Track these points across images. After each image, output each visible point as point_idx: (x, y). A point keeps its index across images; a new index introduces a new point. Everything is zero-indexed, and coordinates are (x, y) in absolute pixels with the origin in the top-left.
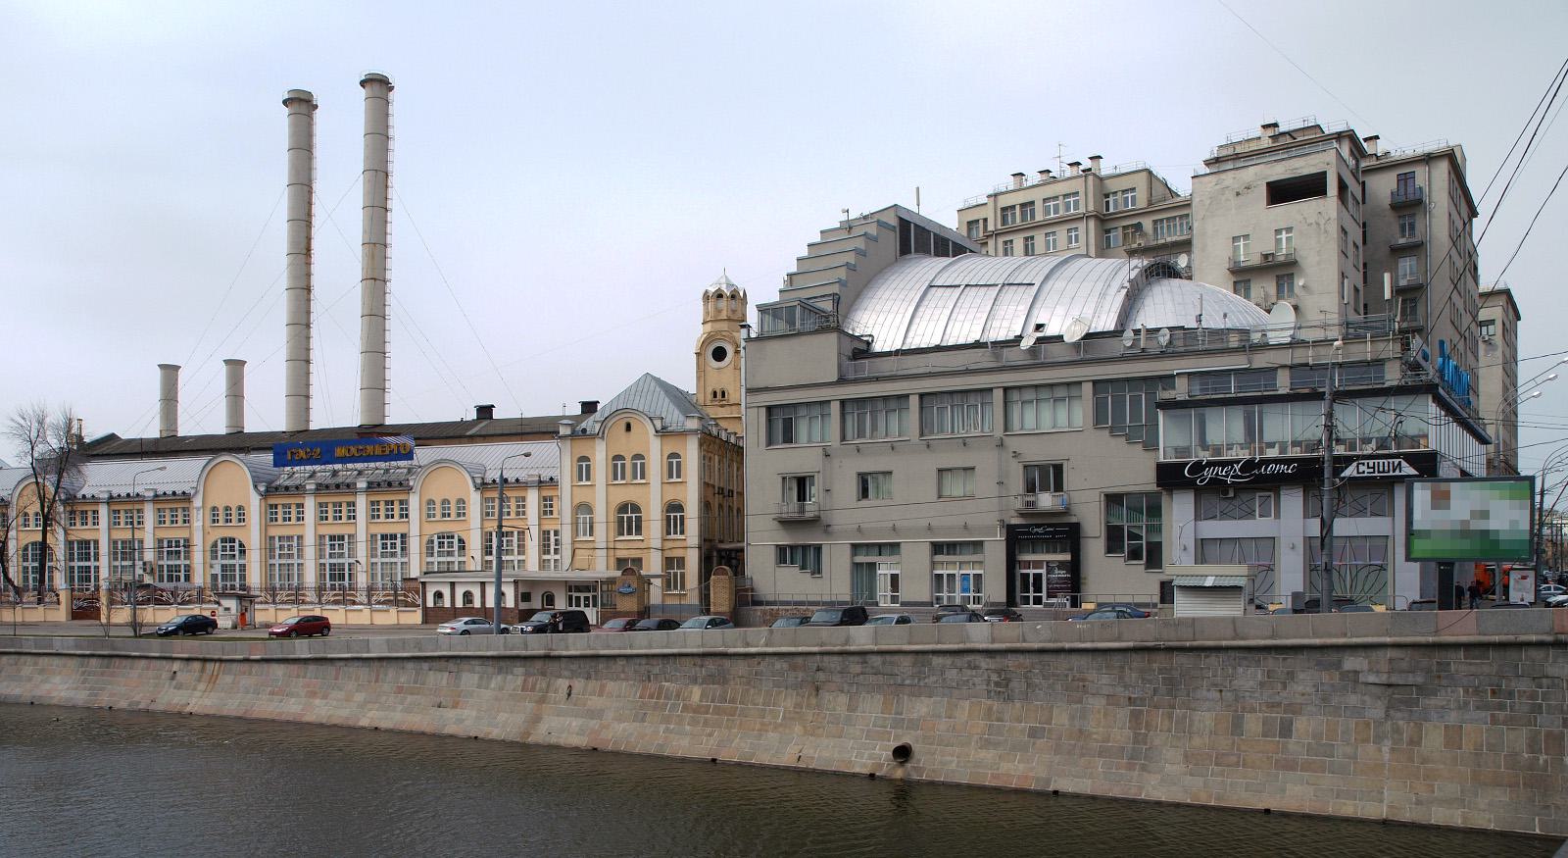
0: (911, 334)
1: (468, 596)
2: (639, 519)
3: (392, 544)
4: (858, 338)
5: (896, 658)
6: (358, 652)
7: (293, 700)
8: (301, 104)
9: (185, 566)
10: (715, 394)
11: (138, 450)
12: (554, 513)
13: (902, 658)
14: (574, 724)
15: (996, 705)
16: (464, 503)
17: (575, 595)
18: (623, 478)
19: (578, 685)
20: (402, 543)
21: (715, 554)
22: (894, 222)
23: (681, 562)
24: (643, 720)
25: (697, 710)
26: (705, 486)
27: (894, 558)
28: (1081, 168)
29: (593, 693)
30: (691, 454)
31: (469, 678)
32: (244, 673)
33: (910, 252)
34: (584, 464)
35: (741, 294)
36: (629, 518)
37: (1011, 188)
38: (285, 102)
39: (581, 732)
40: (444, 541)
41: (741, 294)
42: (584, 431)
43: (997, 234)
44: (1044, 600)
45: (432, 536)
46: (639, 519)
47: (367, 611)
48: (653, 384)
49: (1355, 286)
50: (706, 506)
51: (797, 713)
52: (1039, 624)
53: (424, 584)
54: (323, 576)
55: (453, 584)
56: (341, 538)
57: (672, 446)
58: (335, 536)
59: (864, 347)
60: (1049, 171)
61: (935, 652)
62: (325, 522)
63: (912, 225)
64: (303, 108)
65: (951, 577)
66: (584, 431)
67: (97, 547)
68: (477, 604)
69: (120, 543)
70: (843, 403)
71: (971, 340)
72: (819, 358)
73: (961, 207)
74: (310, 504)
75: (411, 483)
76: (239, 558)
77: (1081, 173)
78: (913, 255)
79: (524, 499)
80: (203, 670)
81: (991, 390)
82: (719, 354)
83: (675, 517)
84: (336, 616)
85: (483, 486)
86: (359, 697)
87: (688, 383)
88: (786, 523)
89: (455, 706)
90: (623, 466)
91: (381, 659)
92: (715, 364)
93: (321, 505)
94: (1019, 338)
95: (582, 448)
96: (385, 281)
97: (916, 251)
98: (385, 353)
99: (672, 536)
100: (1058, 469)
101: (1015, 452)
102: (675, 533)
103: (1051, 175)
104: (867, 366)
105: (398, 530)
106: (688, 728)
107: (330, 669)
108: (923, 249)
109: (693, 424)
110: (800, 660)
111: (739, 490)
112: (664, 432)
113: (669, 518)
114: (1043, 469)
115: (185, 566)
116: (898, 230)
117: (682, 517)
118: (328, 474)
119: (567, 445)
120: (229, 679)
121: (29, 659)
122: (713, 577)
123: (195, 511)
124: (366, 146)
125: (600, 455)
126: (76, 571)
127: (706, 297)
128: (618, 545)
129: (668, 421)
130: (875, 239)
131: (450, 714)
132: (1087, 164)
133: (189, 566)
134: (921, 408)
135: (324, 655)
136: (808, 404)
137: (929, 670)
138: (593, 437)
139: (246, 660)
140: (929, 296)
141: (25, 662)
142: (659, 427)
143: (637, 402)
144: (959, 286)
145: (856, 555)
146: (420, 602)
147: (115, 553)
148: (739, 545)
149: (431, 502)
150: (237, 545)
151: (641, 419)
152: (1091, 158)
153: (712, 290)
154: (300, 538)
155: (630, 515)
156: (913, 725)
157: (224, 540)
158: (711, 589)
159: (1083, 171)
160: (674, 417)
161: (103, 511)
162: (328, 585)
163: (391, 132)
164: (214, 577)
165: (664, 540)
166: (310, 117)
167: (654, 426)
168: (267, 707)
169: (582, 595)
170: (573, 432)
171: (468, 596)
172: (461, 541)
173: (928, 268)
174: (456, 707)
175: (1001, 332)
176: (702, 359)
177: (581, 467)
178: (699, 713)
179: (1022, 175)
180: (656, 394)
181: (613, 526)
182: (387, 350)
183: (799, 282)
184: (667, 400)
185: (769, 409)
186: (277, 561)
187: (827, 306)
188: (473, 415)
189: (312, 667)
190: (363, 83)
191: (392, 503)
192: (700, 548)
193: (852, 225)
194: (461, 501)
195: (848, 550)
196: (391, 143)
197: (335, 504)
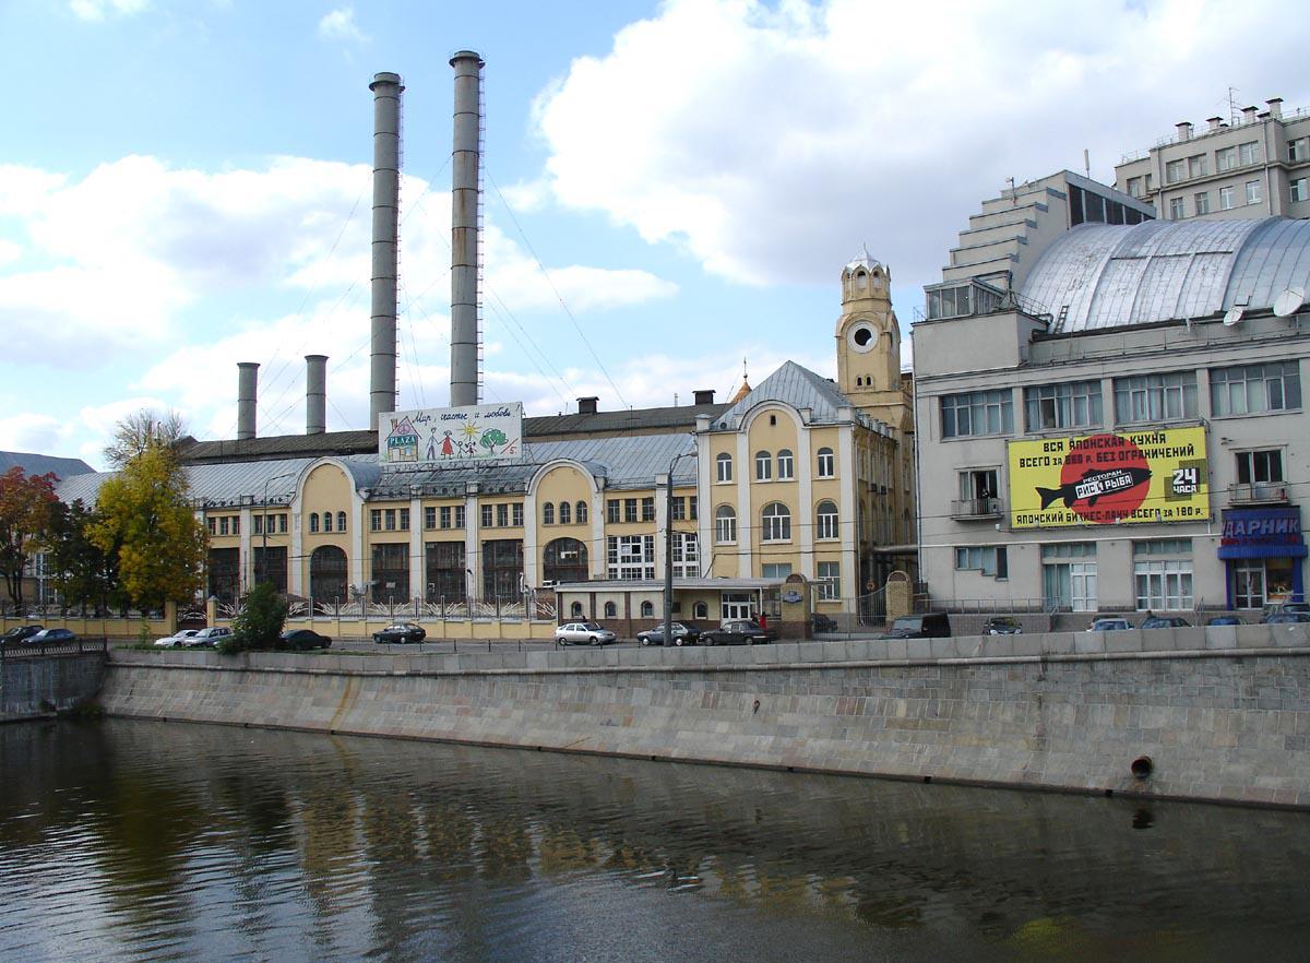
0: (1095, 312)
1: (610, 607)
2: (786, 521)
4: (1036, 318)
5: (1129, 665)
6: (514, 667)
7: (444, 717)
8: (388, 87)
9: (647, 569)
11: (216, 453)
13: (1135, 665)
14: (764, 743)
15: (1245, 715)
16: (586, 506)
17: (730, 604)
18: (768, 476)
19: (766, 701)
21: (871, 558)
22: (1065, 189)
23: (835, 566)
24: (843, 737)
25: (903, 725)
26: (861, 483)
27: (1089, 560)
28: (1258, 113)
29: (784, 709)
30: (844, 446)
31: (641, 696)
32: (387, 690)
34: (724, 462)
36: (776, 520)
37: (1176, 140)
38: (372, 87)
39: (773, 749)
42: (724, 425)
43: (1162, 192)
44: (1265, 602)
46: (787, 522)
47: (495, 623)
48: (797, 373)
49: (1037, 489)
50: (861, 505)
51: (1018, 726)
52: (1290, 626)
53: (560, 594)
55: (593, 595)
57: (823, 439)
59: (1042, 327)
60: (1219, 119)
61: (1171, 658)
63: (1083, 192)
64: (391, 91)
65: (1155, 578)
66: (724, 425)
68: (621, 615)
70: (1026, 390)
71: (1164, 318)
72: (995, 342)
73: (1119, 163)
77: (1258, 119)
78: (1085, 224)
80: (242, 678)
81: (1194, 371)
82: (862, 337)
83: (828, 518)
84: (433, 630)
86: (518, 714)
87: (829, 369)
89: (627, 723)
90: (768, 463)
91: (539, 674)
94: (1221, 314)
95: (722, 444)
96: (476, 267)
97: (1088, 220)
99: (825, 539)
100: (1276, 455)
101: (1224, 439)
102: (828, 535)
103: (1222, 122)
104: (1049, 349)
106: (895, 744)
107: (483, 687)
108: (1095, 216)
109: (846, 415)
110: (1020, 669)
111: (891, 486)
112: (813, 425)
113: (820, 519)
114: (1260, 457)
116: (1068, 197)
117: (733, 522)
120: (371, 695)
121: (158, 672)
122: (889, 583)
124: (457, 126)
125: (742, 452)
127: (846, 276)
128: (818, 548)
129: (816, 412)
130: (1045, 209)
131: (622, 732)
132: (1264, 108)
134: (1116, 394)
136: (1075, 384)
137: (1167, 677)
138: (736, 431)
139: (390, 675)
140: (1111, 271)
141: (155, 677)
142: (807, 421)
143: (779, 392)
144: (1145, 257)
145: (1045, 556)
146: (555, 613)
148: (912, 547)
149: (549, 506)
151: (783, 409)
152: (1269, 102)
153: (853, 266)
155: (776, 516)
156: (1152, 735)
158: (887, 596)
159: (1260, 116)
160: (823, 407)
163: (482, 110)
165: (815, 544)
166: (396, 99)
168: (412, 725)
169: (739, 605)
171: (610, 607)
173: (1112, 237)
174: (629, 726)
175: (1194, 308)
177: (721, 465)
178: (906, 728)
179: (1189, 124)
180: (801, 384)
181: (758, 533)
182: (479, 340)
183: (964, 258)
184: (813, 390)
185: (943, 399)
187: (1000, 284)
189: (462, 682)
190: (453, 62)
191: (433, 509)
192: (856, 551)
193: (1018, 193)
194: (581, 505)
195: (1036, 552)
196: (482, 121)
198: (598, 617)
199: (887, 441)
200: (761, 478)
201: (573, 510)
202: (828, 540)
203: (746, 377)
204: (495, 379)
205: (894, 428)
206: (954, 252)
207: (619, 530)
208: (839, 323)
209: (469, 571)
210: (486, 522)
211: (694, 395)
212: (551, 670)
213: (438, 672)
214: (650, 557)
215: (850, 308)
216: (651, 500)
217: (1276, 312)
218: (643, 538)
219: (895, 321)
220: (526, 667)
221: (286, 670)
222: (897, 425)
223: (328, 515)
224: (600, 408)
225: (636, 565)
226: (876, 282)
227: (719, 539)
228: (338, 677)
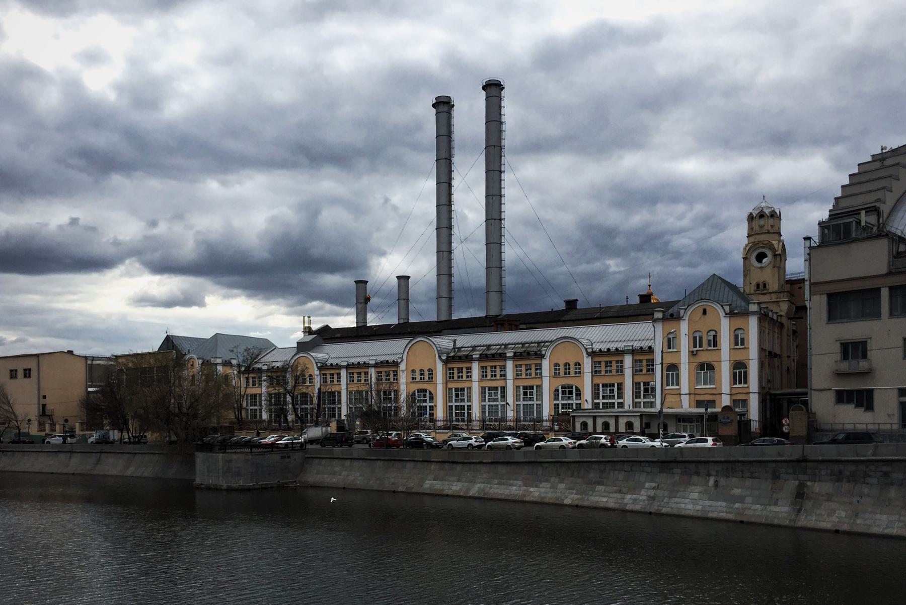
3: (530, 392)
9: (468, 406)
10: (758, 286)
12: (464, 377)
16: (580, 365)
18: (701, 346)
19: (722, 481)
20: (618, 389)
26: (761, 350)
33: (433, 413)
35: (778, 214)
40: (568, 391)
41: (778, 214)
45: (558, 387)
53: (574, 417)
54: (518, 412)
56: (532, 388)
57: (739, 322)
58: (527, 387)
62: (461, 379)
64: (493, 90)
66: (672, 315)
67: (340, 396)
69: (642, 384)
74: (476, 367)
75: (543, 353)
76: (429, 403)
79: (470, 368)
82: (760, 257)
83: (740, 372)
85: (593, 354)
88: (840, 375)
92: (759, 265)
93: (483, 367)
95: (671, 327)
98: (501, 268)
102: (673, 384)
105: (499, 384)
112: (731, 314)
115: (468, 406)
117: (746, 373)
118: (485, 347)
119: (659, 326)
123: (401, 372)
126: (454, 409)
127: (751, 218)
133: (470, 406)
135: (535, 460)
147: (451, 397)
148: (845, 400)
150: (428, 394)
154: (470, 388)
157: (419, 391)
161: (344, 373)
162: (454, 419)
164: (413, 413)
165: (731, 388)
167: (724, 310)
168: (497, 490)
170: (664, 315)
172: (430, 393)
176: (747, 261)
183: (845, 203)
186: (601, 401)
188: (563, 306)
197: (358, 373)
198: (576, 431)
199: (777, 324)
200: (696, 347)
201: (426, 373)
202: (741, 386)
203: (650, 286)
204: (813, 392)
205: (781, 316)
206: (836, 199)
207: (600, 381)
208: (745, 249)
209: (586, 400)
210: (484, 376)
211: (639, 297)
212: (582, 460)
213: (511, 461)
214: (620, 396)
215: (389, 251)
216: (622, 362)
217: (809, 252)
218: (616, 385)
219: (783, 246)
220: (566, 458)
221: (416, 459)
222: (783, 314)
223: (422, 371)
224: (579, 306)
225: (462, 404)
226: (771, 221)
227: (735, 383)
228: (448, 464)
